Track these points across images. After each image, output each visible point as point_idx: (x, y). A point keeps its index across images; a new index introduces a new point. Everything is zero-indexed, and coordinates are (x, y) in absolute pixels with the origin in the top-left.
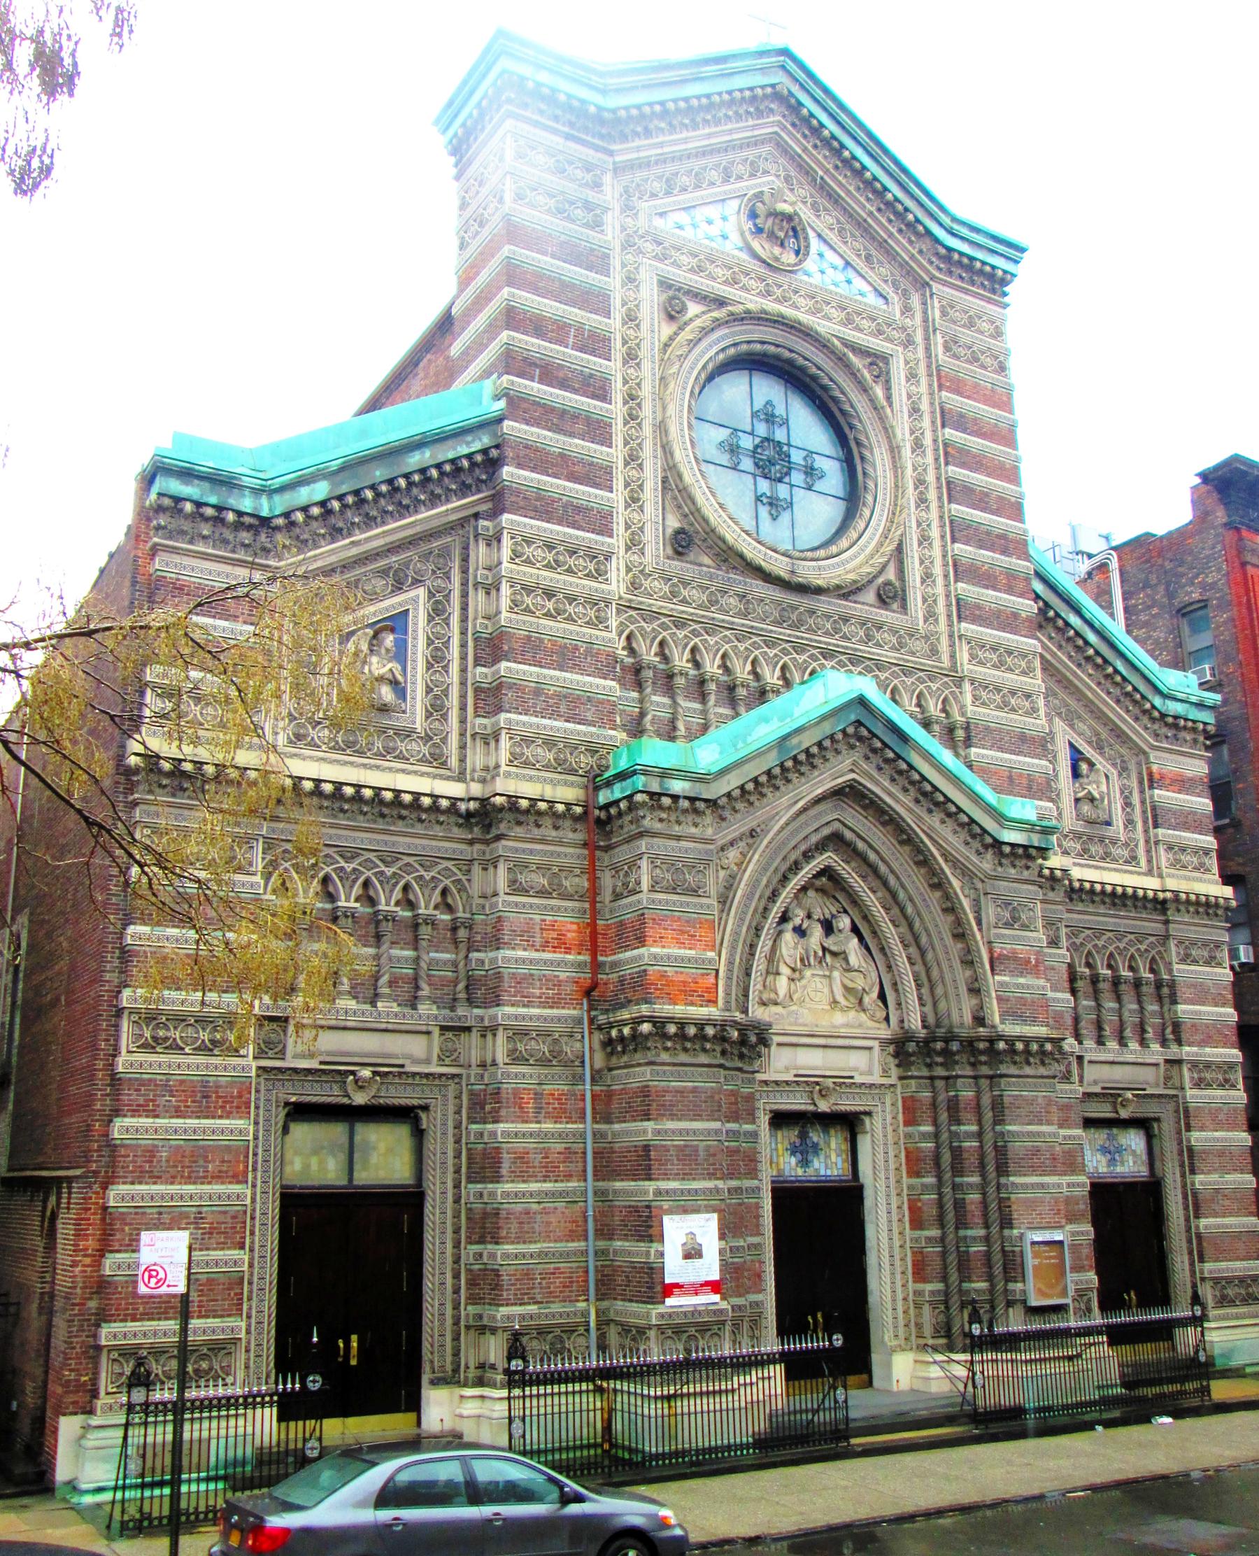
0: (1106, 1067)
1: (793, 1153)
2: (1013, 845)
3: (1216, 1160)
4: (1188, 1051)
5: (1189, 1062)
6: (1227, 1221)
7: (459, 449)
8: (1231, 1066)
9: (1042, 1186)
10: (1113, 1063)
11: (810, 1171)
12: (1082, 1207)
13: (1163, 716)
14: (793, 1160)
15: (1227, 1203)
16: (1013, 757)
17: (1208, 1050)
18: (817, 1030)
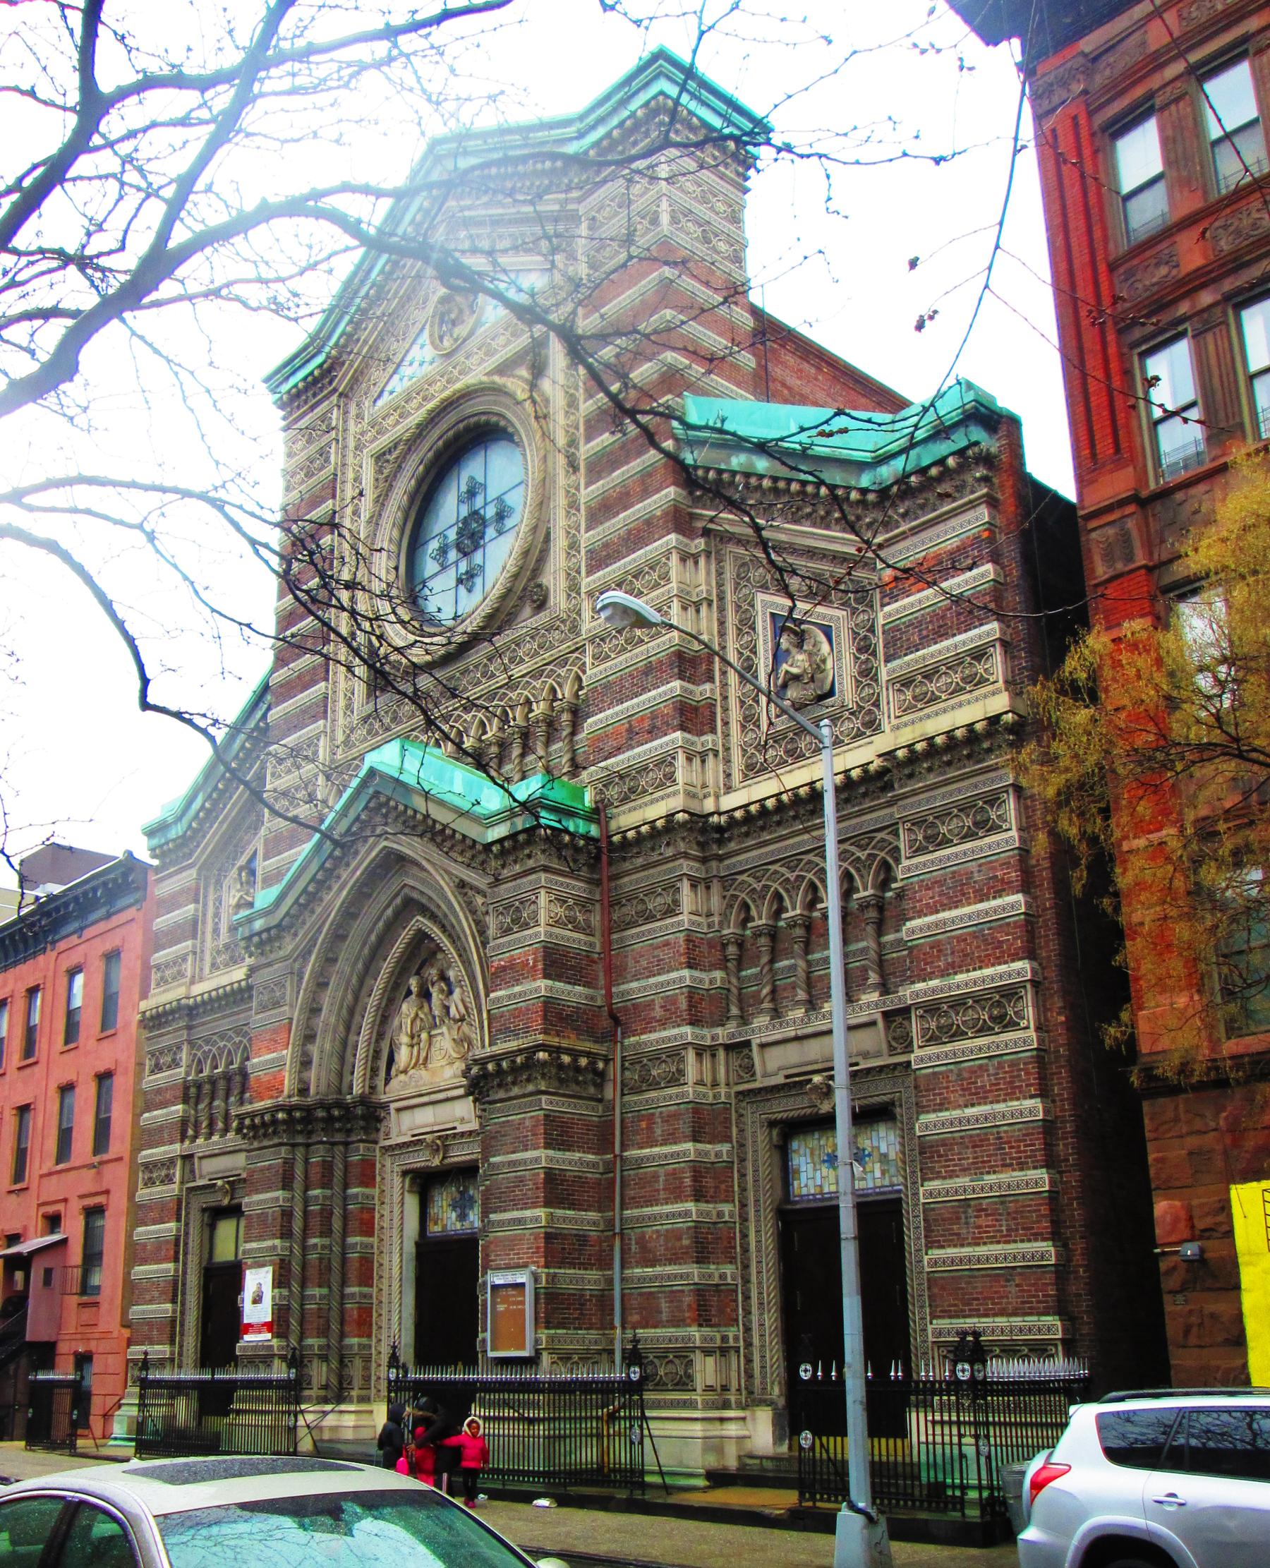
0: (792, 1048)
1: (454, 1208)
2: (500, 841)
3: (969, 1153)
4: (914, 991)
5: (918, 1006)
6: (982, 1250)
7: (1163, 396)
8: (1010, 993)
9: (519, 1221)
10: (797, 1038)
11: (467, 1224)
12: (686, 1242)
13: (883, 493)
14: (454, 1215)
15: (983, 1221)
16: (635, 701)
17: (960, 977)
18: (424, 1089)
